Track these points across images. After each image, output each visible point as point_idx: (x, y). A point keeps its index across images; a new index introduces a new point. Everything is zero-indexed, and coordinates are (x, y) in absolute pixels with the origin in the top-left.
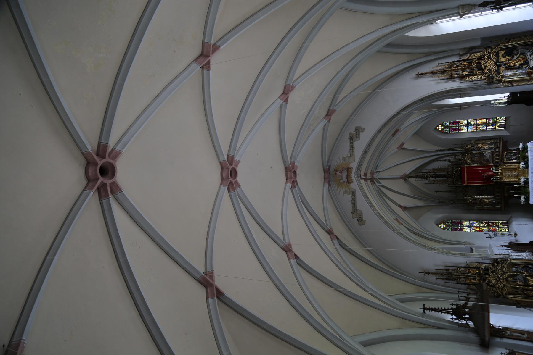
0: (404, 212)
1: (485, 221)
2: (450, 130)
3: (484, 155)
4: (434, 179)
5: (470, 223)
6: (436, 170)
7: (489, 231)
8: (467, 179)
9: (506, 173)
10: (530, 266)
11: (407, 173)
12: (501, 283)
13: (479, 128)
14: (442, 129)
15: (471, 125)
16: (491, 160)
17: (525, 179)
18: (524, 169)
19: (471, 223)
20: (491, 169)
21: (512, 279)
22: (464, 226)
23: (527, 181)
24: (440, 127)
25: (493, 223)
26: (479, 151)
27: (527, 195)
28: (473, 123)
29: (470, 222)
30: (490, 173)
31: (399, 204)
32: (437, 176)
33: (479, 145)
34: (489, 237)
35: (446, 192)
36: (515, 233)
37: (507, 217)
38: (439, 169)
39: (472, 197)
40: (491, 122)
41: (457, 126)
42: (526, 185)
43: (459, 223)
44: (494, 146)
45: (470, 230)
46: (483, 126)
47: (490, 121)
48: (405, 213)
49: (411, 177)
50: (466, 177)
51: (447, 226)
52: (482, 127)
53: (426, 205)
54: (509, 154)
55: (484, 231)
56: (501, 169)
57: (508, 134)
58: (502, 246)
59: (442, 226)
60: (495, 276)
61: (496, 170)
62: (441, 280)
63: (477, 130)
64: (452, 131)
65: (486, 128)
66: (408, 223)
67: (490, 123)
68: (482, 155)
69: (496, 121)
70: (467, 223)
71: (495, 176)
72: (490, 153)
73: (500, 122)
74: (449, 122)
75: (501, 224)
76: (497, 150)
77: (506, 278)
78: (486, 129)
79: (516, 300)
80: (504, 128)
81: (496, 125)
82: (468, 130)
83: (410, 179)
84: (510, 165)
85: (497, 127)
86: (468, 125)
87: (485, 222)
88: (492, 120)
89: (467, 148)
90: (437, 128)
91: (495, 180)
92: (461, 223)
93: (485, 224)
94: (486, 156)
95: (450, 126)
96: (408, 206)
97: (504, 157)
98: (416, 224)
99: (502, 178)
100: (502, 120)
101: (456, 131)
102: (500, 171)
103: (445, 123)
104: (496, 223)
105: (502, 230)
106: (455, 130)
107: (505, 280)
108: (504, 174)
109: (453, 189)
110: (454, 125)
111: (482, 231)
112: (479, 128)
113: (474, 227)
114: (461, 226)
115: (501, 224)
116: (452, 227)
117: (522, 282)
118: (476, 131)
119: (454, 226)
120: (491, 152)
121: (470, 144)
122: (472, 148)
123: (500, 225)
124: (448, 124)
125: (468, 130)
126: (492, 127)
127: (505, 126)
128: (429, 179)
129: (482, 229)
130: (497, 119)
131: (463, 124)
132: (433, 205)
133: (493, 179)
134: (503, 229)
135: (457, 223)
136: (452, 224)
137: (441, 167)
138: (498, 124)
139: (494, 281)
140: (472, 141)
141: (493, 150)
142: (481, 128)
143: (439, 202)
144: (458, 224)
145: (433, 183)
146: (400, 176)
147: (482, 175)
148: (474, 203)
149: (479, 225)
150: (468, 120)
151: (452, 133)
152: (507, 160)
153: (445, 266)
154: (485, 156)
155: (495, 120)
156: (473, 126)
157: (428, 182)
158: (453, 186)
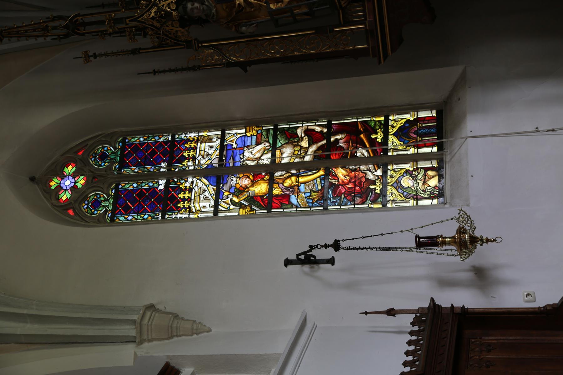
1: (311, 125)
22: (185, 173)
29: (223, 138)
34: (302, 257)
36: (461, 230)
43: (164, 153)
48: (202, 69)
55: (293, 199)
75: (402, 133)
87: (309, 133)
93: (305, 144)
104: (369, 129)
105: (407, 182)
113: (244, 170)
114: (169, 176)
115: (402, 133)
116: (125, 186)
129: (288, 183)
134: (407, 172)
135: (153, 153)
144: (158, 162)
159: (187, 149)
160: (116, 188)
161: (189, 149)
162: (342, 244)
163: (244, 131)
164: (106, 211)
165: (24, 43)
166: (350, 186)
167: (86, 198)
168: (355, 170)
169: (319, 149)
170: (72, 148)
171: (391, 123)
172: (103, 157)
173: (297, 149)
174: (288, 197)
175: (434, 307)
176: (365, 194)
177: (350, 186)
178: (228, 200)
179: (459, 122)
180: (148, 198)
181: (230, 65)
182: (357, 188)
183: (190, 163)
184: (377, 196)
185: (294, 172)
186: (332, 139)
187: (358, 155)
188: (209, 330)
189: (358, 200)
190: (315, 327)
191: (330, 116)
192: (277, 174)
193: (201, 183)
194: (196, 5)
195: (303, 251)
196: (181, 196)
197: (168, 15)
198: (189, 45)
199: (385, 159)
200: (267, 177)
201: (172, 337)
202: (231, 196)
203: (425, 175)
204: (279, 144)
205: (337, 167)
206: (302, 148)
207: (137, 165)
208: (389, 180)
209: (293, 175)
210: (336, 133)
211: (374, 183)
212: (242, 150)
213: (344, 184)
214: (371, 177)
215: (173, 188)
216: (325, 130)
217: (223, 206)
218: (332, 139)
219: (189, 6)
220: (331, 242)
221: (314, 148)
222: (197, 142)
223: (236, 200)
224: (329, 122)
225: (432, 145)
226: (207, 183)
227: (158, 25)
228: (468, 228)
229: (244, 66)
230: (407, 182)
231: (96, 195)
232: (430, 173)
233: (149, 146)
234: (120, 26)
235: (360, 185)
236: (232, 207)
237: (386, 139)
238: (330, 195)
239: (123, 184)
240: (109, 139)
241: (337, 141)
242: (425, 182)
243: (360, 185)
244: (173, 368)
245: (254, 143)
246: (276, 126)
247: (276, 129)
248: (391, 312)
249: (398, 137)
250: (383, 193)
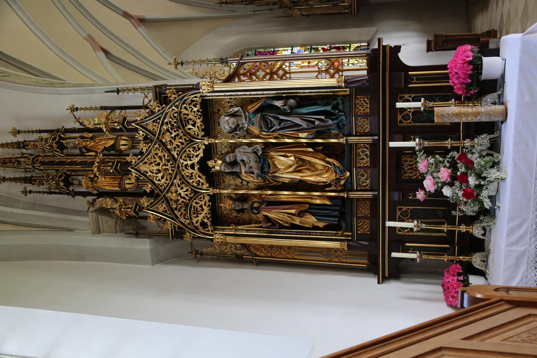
0: (136, 28)
1: (324, 47)
10: (279, 103)
12: (184, 181)
21: (220, 162)
29: (292, 50)
31: (123, 10)
60: (160, 158)
62: (13, 183)
66: (137, 52)
77: (198, 163)
79: (245, 246)
87: (323, 49)
98: (163, 57)
107: (196, 168)
117: (253, 173)
132: (216, 15)
139: (160, 175)
153: (17, 132)
163: (300, 48)
170: (237, 52)
171: (351, 46)
176: (432, 161)
191: (331, 44)
195: (104, 105)
198: (290, 8)
222: (282, 51)
224: (330, 46)
246: (311, 47)
247: (311, 48)
249: (309, 190)
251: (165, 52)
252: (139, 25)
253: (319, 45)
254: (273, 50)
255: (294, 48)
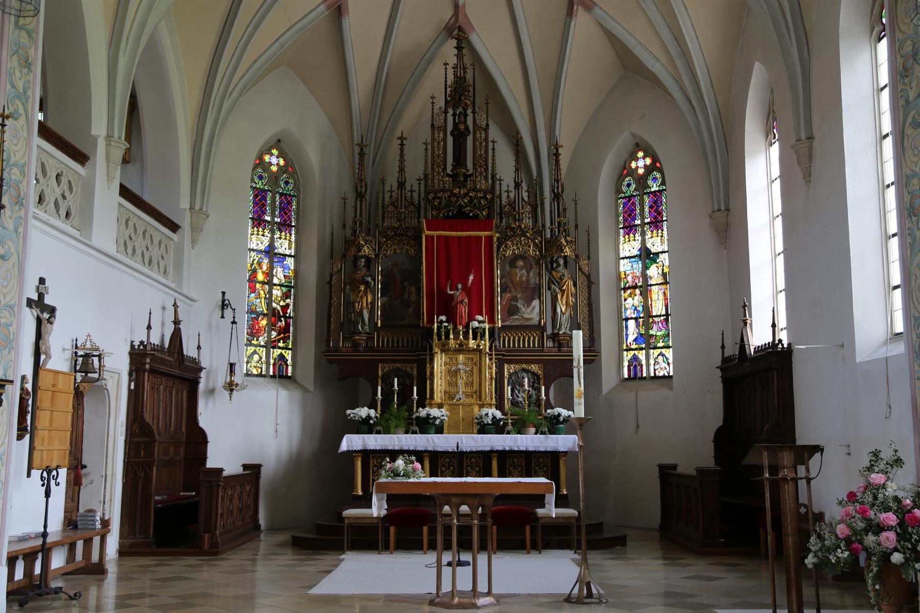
1: (291, 307)
2: (630, 197)
3: (533, 299)
4: (450, 127)
5: (285, 255)
6: (483, 136)
7: (251, 311)
8: (446, 237)
9: (464, 364)
11: (474, 39)
13: (630, 295)
14: (632, 173)
15: (646, 268)
16: (514, 324)
17: (437, 422)
18: (476, 421)
19: (284, 259)
20: (480, 318)
22: (272, 232)
23: (433, 430)
24: (641, 164)
25: (286, 330)
26: (551, 282)
27: (379, 428)
28: (654, 272)
29: (290, 256)
30: (464, 310)
32: (460, 136)
33: (571, 283)
34: (227, 302)
35: (402, 169)
36: (237, 385)
37: (308, 374)
38: (487, 146)
39: (377, 256)
40: (651, 332)
41: (643, 218)
42: (417, 425)
43: (285, 221)
44: (565, 333)
45: (260, 252)
46: (640, 309)
47: (655, 327)
48: (318, 6)
49: (459, 48)
50: (454, 234)
51: (274, 178)
52: (636, 302)
53: (354, 114)
54: (533, 383)
55: (253, 295)
56: (478, 346)
57: (606, 388)
58: (177, 322)
59: (274, 161)
61: (475, 331)
63: (625, 289)
64: (625, 204)
65: (632, 318)
67: (648, 327)
68: (534, 292)
69: (655, 348)
70: (284, 246)
71: (455, 328)
72: (540, 322)
73: (652, 362)
74: (660, 191)
75: (282, 357)
76: (550, 344)
78: (627, 319)
80: (626, 376)
81: (641, 349)
82: (626, 258)
83: (449, 50)
84: (491, 378)
85: (632, 352)
86: (647, 256)
87: (288, 306)
88: (659, 333)
89: (563, 240)
90: (640, 154)
91: (439, 328)
92: (284, 226)
93: (282, 303)
94: (528, 307)
95: (646, 197)
96: (346, 23)
97: (524, 366)
99: (445, 349)
100: (656, 368)
101: (625, 220)
102: (472, 343)
103: (658, 175)
104: (285, 340)
105: (256, 357)
106: (629, 215)
108: (461, 358)
109: (412, 196)
110: (647, 209)
111: (253, 289)
112: (630, 295)
113: (271, 268)
114: (272, 223)
115: (282, 357)
116: (269, 195)
118: (622, 287)
119: (273, 198)
120: (545, 324)
121: (577, 256)
122: (562, 262)
123: (277, 352)
124: (655, 188)
125: (626, 258)
126: (631, 338)
127: (635, 377)
128: (451, 111)
129: (262, 292)
130: (663, 351)
131: (651, 240)
132: (355, 135)
133: (442, 322)
134: (261, 358)
135: (286, 214)
136: (281, 195)
137: (493, 153)
138: (642, 355)
140: (586, 262)
141: (549, 331)
142: (633, 302)
143: (362, 146)
144: (281, 216)
145: (432, 125)
146: (464, 5)
147: (460, 286)
148: (356, 259)
149: (275, 285)
150: (666, 255)
151: (617, 206)
152: (510, 375)
154: (528, 303)
155: (660, 344)
156: (638, 274)
157: (440, 108)
158: (419, 193)
159: (286, 234)
160: (269, 190)
161: (286, 236)
162: (234, 325)
163: (293, 269)
164: (256, 183)
165: (357, 161)
166: (257, 327)
167: (265, 171)
168: (265, 330)
169: (278, 311)
171: (287, 351)
172: (287, 183)
173: (279, 299)
174: (254, 292)
175: (201, 369)
177: (257, 327)
178: (255, 257)
179: (285, 387)
180: (261, 210)
181: (331, 276)
182: (255, 331)
183: (278, 236)
184: (250, 341)
185: (267, 296)
186: (282, 319)
187: (273, 332)
188: (193, 248)
189: (249, 331)
190: (191, 306)
192: (267, 286)
193: (266, 241)
194: (363, 264)
196: (260, 229)
197: (360, 250)
198: (344, 256)
199: (269, 347)
200: (266, 281)
201: (192, 228)
202: (257, 259)
203: (259, 367)
204: (283, 288)
205: (268, 320)
206: (280, 301)
207: (280, 204)
208: (258, 348)
209: (266, 295)
210: (286, 321)
211: (257, 340)
212: (283, 267)
213: (258, 324)
214: (260, 339)
215: (265, 225)
216: (288, 315)
217: (253, 254)
218: (282, 319)
219: (363, 260)
220: (236, 320)
221: (279, 308)
222: (289, 240)
223: (255, 262)
224: (292, 318)
225: (274, 372)
226: (266, 245)
227: (356, 243)
228: (238, 388)
229: (330, 283)
230: (256, 357)
231: (266, 177)
232: (260, 370)
233: (290, 211)
234: (358, 223)
235: (257, 332)
236: (252, 259)
237: (280, 348)
238: (253, 316)
239: (271, 194)
240: (297, 188)
241: (281, 321)
242: (255, 367)
243: (257, 332)
244: (177, 230)
245: (285, 274)
246: (293, 287)
247: (291, 287)
248: (199, 347)
250: (251, 345)
251: (282, 46)
252: (329, 7)
253: (294, 299)
254: (293, 224)
255: (293, 258)
